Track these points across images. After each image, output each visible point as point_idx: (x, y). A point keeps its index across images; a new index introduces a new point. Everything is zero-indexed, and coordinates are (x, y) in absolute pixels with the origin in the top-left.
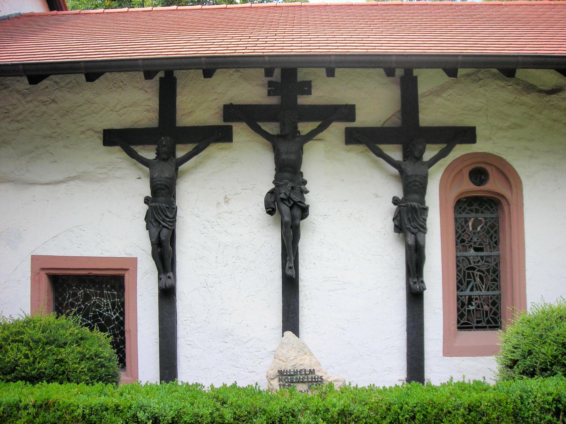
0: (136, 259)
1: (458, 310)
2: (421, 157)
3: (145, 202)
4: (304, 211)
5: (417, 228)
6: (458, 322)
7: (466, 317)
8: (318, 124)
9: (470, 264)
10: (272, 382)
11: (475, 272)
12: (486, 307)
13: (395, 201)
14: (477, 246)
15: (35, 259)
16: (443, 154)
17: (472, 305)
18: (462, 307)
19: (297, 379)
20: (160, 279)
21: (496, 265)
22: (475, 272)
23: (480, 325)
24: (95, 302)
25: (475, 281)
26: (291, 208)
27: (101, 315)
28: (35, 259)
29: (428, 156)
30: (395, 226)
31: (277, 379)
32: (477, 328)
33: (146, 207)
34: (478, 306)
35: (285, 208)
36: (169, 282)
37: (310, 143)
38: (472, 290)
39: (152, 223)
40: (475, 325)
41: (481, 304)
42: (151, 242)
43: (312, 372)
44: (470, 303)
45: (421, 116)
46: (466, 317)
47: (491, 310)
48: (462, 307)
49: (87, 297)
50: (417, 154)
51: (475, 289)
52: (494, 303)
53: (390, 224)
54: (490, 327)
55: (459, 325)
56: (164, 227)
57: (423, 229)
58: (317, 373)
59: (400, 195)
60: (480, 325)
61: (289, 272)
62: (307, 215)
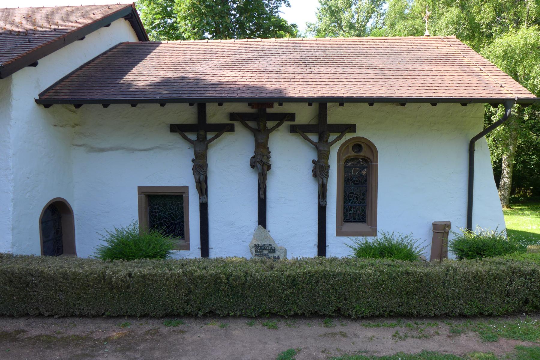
0: (188, 187)
1: (344, 213)
2: (327, 141)
3: (192, 162)
4: (269, 167)
5: (323, 176)
6: (344, 219)
7: (348, 216)
8: (277, 122)
9: (351, 190)
10: (252, 249)
11: (354, 195)
12: (358, 212)
13: (314, 162)
14: (355, 182)
15: (140, 188)
16: (339, 138)
17: (352, 211)
18: (347, 212)
19: (263, 248)
20: (200, 199)
21: (365, 191)
22: (354, 195)
23: (355, 220)
24: (169, 207)
25: (353, 199)
26: (262, 166)
27: (172, 213)
28: (140, 188)
29: (331, 139)
30: (313, 174)
31: (254, 248)
32: (354, 222)
33: (192, 164)
34: (355, 212)
35: (259, 165)
36: (204, 200)
37: (274, 132)
38: (352, 203)
39: (196, 172)
40: (353, 220)
41: (356, 210)
42: (196, 181)
43: (270, 245)
44: (350, 210)
45: (328, 119)
46: (348, 216)
47: (361, 213)
48: (347, 212)
49: (165, 205)
50: (325, 140)
51: (353, 203)
52: (363, 210)
53: (311, 173)
54: (360, 222)
55: (344, 220)
56: (201, 174)
57: (327, 176)
58: (272, 246)
59: (316, 160)
60: (355, 220)
61: (262, 196)
62: (270, 169)
